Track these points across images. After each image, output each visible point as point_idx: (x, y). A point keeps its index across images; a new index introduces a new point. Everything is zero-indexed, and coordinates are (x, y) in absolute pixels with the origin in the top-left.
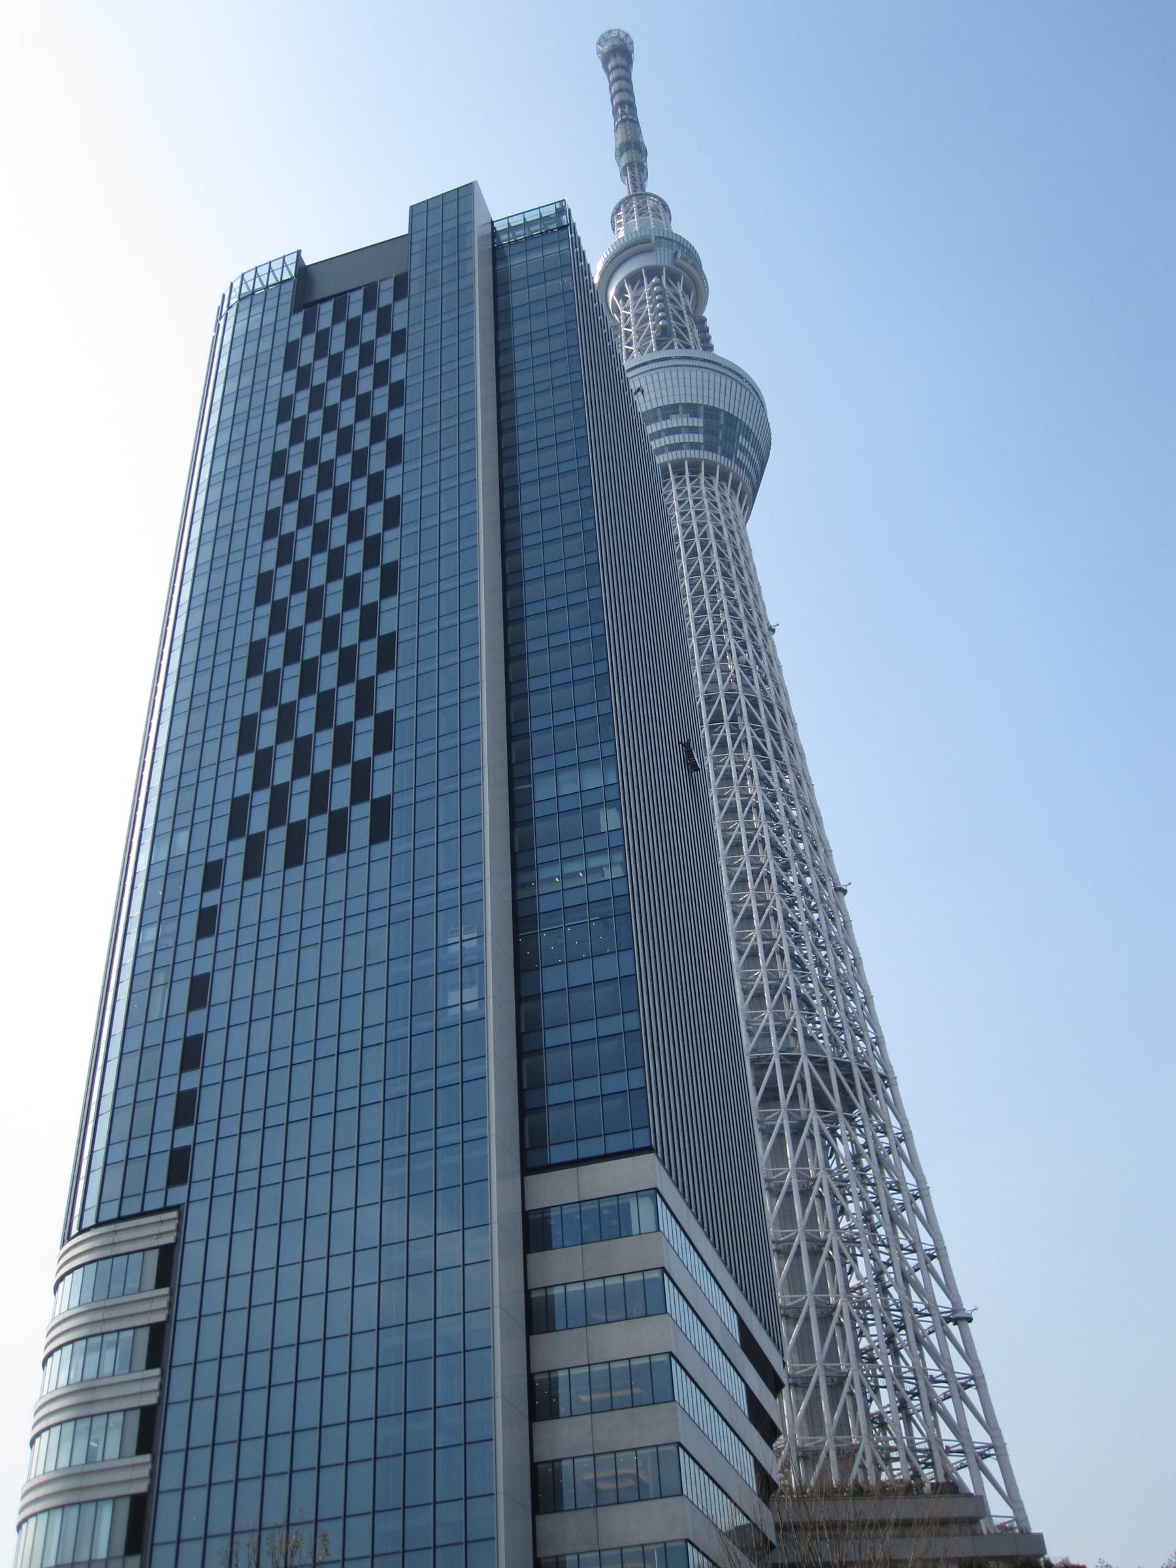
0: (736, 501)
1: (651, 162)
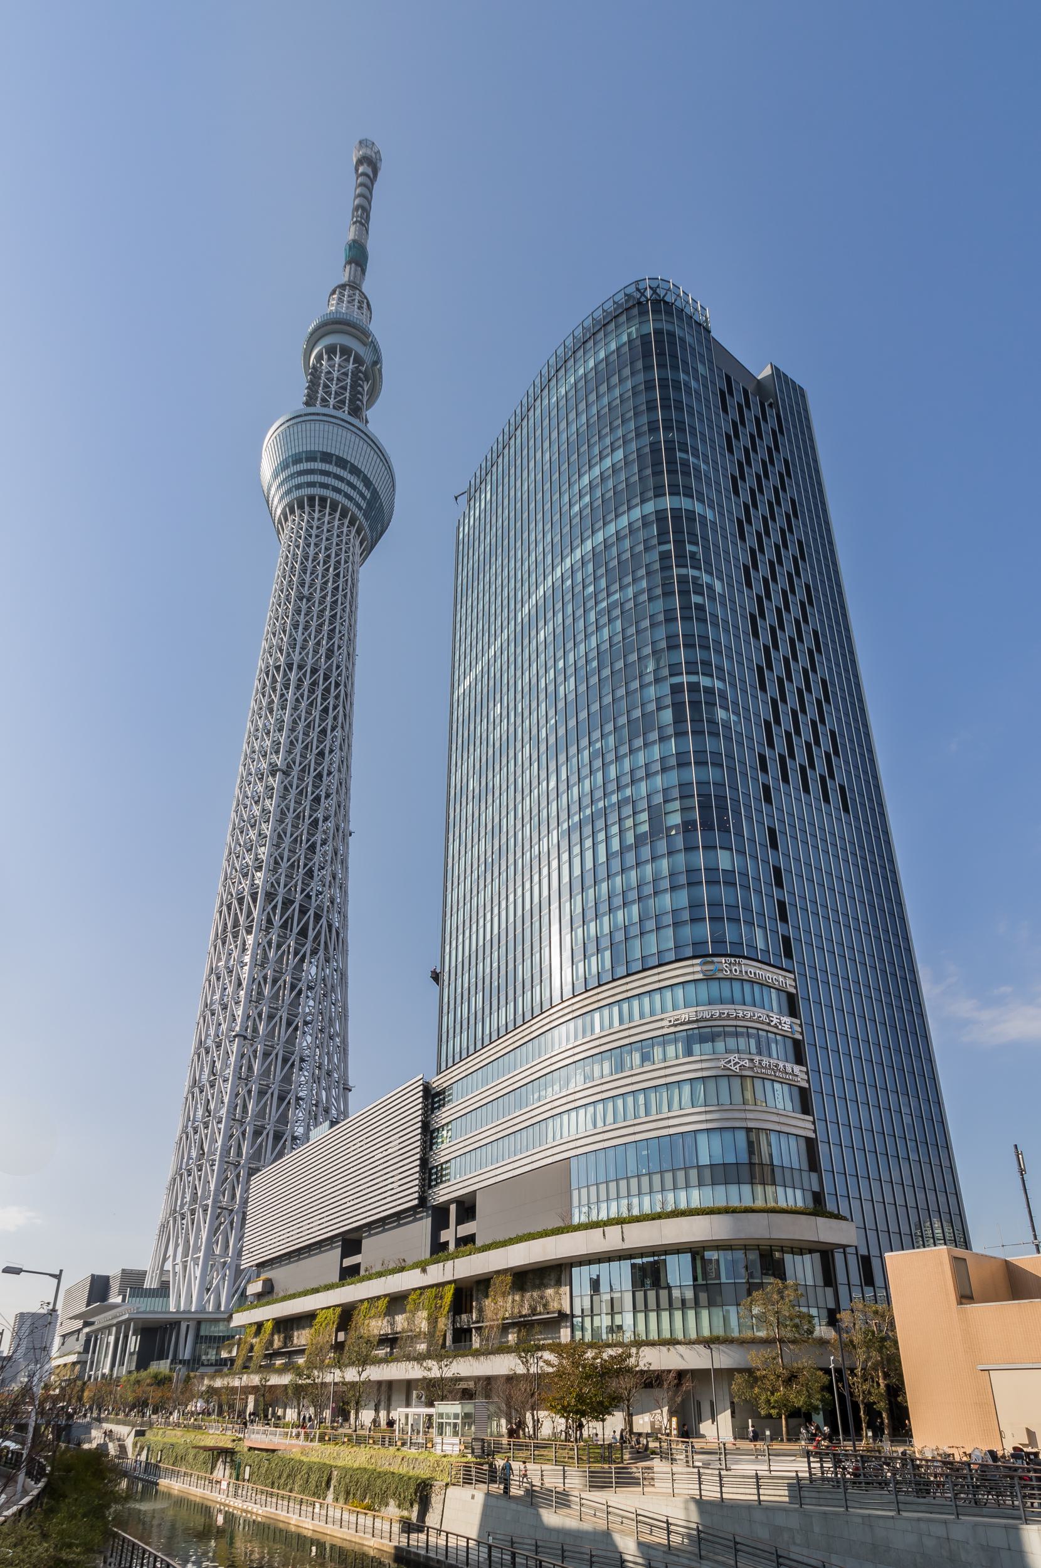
0: (357, 543)
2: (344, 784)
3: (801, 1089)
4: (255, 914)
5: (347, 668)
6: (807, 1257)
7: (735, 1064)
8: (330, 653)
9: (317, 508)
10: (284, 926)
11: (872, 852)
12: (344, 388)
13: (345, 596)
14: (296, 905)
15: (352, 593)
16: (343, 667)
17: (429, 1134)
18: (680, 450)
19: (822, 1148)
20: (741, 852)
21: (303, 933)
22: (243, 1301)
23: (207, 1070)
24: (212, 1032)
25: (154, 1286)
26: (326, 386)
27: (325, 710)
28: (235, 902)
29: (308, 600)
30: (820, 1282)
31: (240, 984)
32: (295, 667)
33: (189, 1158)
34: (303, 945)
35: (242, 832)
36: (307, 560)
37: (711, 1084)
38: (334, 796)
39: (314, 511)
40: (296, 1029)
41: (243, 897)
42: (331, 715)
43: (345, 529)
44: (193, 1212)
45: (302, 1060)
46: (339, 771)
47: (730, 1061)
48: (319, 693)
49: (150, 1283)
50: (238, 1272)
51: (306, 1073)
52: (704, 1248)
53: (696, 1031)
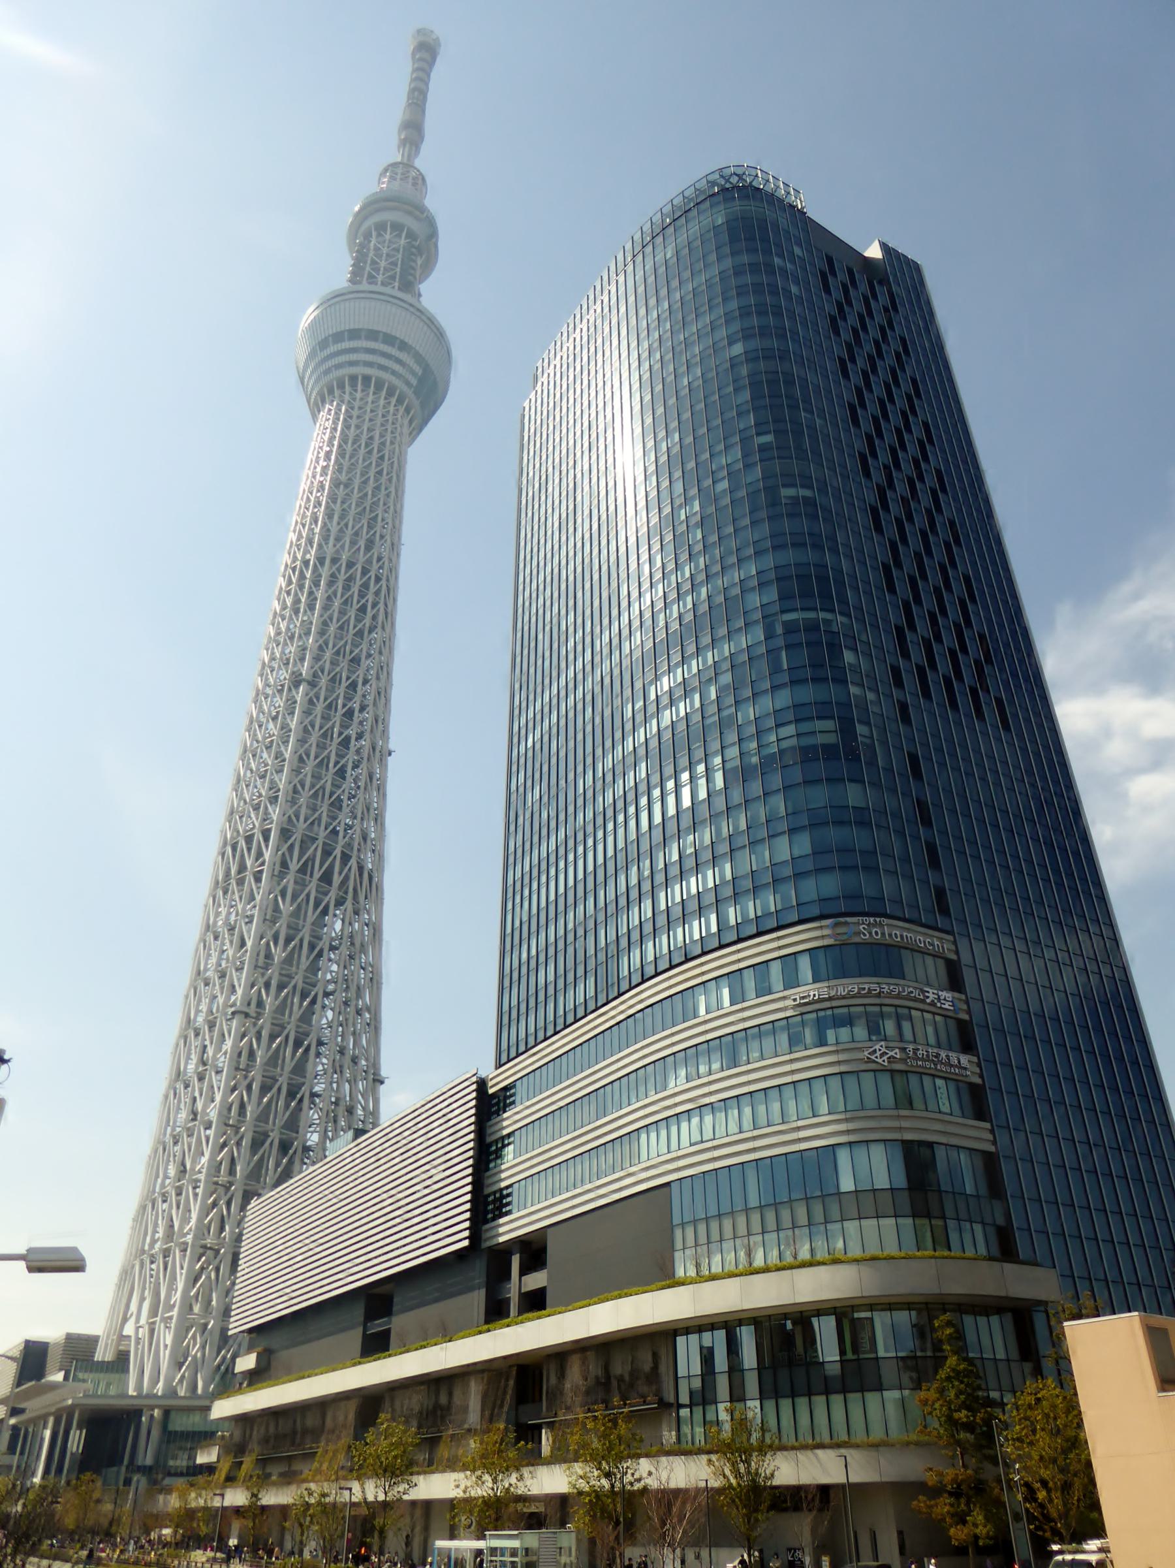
0: (406, 422)
1: (425, 148)
2: (383, 694)
3: (972, 1086)
4: (267, 855)
5: (390, 560)
6: (995, 1320)
7: (882, 1055)
8: (370, 545)
9: (359, 387)
10: (302, 870)
11: (1070, 875)
12: (395, 264)
13: (390, 480)
14: (320, 842)
15: (398, 476)
16: (386, 560)
17: (487, 1152)
18: (860, 722)
19: (1005, 1168)
20: (876, 785)
21: (327, 878)
22: (228, 1382)
23: (194, 1058)
24: (204, 1007)
25: (109, 1357)
26: (374, 262)
27: (363, 609)
28: (242, 843)
29: (346, 486)
30: (1014, 1354)
31: (243, 944)
32: (339, 501)
33: (166, 1177)
34: (326, 894)
35: (254, 756)
36: (346, 443)
37: (851, 1081)
38: (370, 708)
39: (356, 391)
40: (313, 1002)
41: (253, 835)
42: (370, 613)
43: (392, 409)
44: (166, 1253)
45: (320, 1043)
46: (378, 678)
47: (875, 1051)
48: (355, 589)
49: (103, 1354)
50: (224, 1339)
51: (325, 1061)
52: (854, 1308)
53: (829, 1012)
